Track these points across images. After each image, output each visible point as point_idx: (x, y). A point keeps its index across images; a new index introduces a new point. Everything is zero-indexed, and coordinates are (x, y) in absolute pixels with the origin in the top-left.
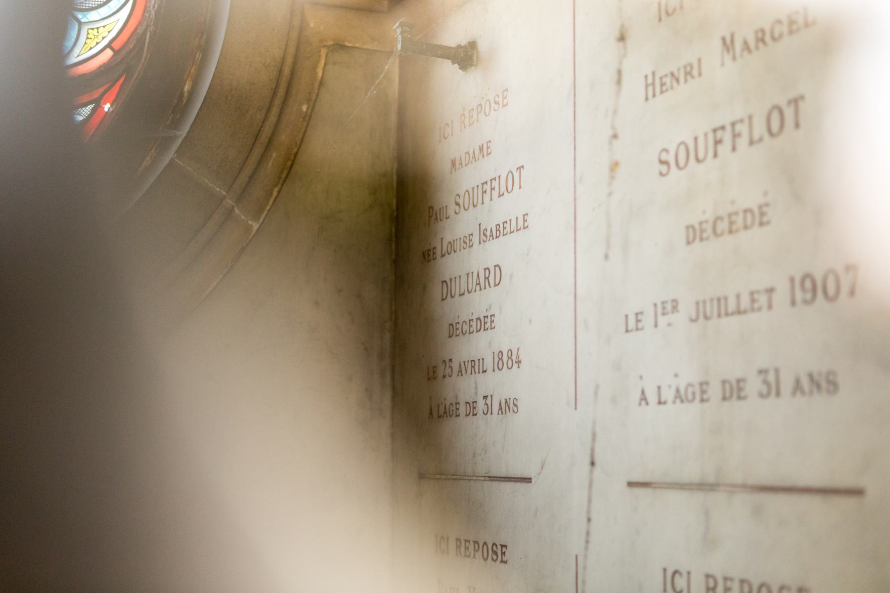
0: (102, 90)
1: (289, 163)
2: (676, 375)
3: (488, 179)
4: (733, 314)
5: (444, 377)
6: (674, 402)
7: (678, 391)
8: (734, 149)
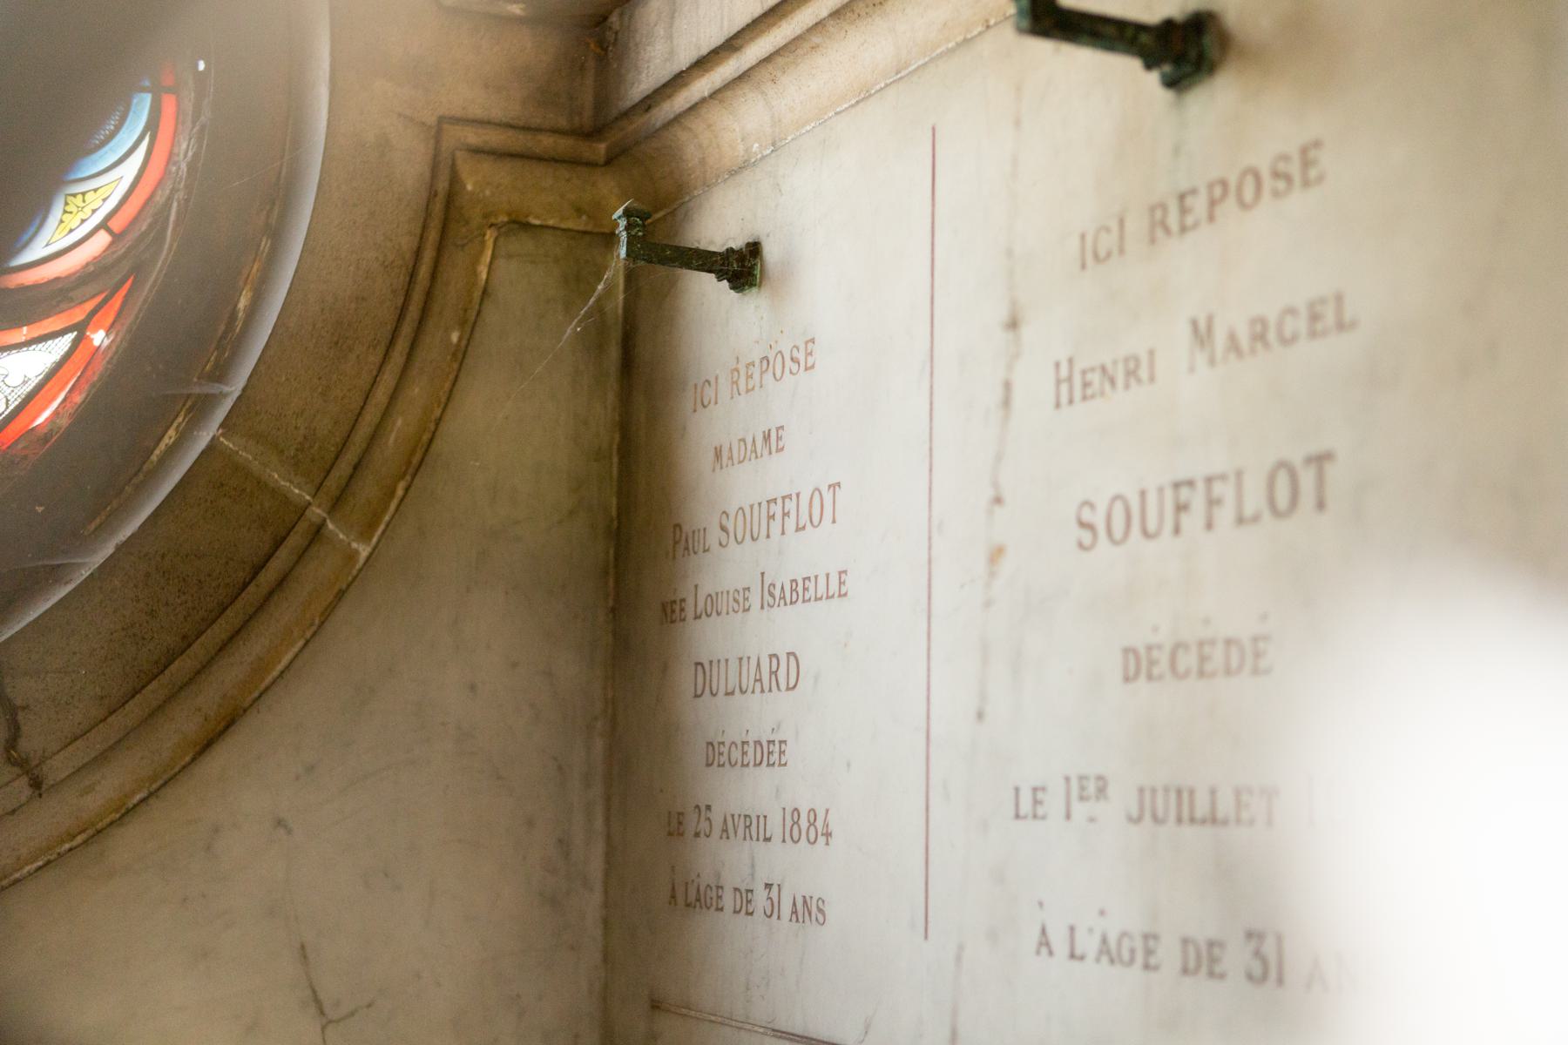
0: (89, 306)
1: (426, 437)
2: (1102, 913)
3: (778, 494)
4: (1203, 821)
5: (697, 835)
6: (1098, 960)
7: (1104, 941)
8: (1209, 526)
